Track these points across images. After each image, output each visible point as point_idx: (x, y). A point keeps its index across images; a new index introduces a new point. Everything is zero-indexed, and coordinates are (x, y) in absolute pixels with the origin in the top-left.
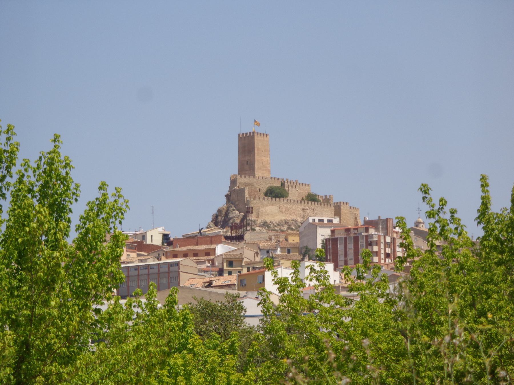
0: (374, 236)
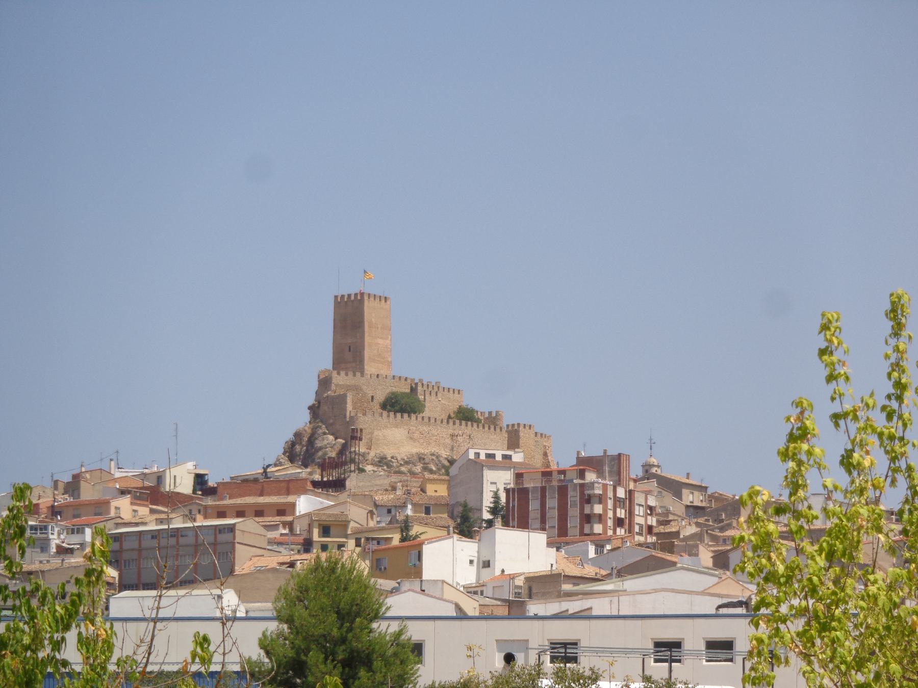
0: (596, 485)
